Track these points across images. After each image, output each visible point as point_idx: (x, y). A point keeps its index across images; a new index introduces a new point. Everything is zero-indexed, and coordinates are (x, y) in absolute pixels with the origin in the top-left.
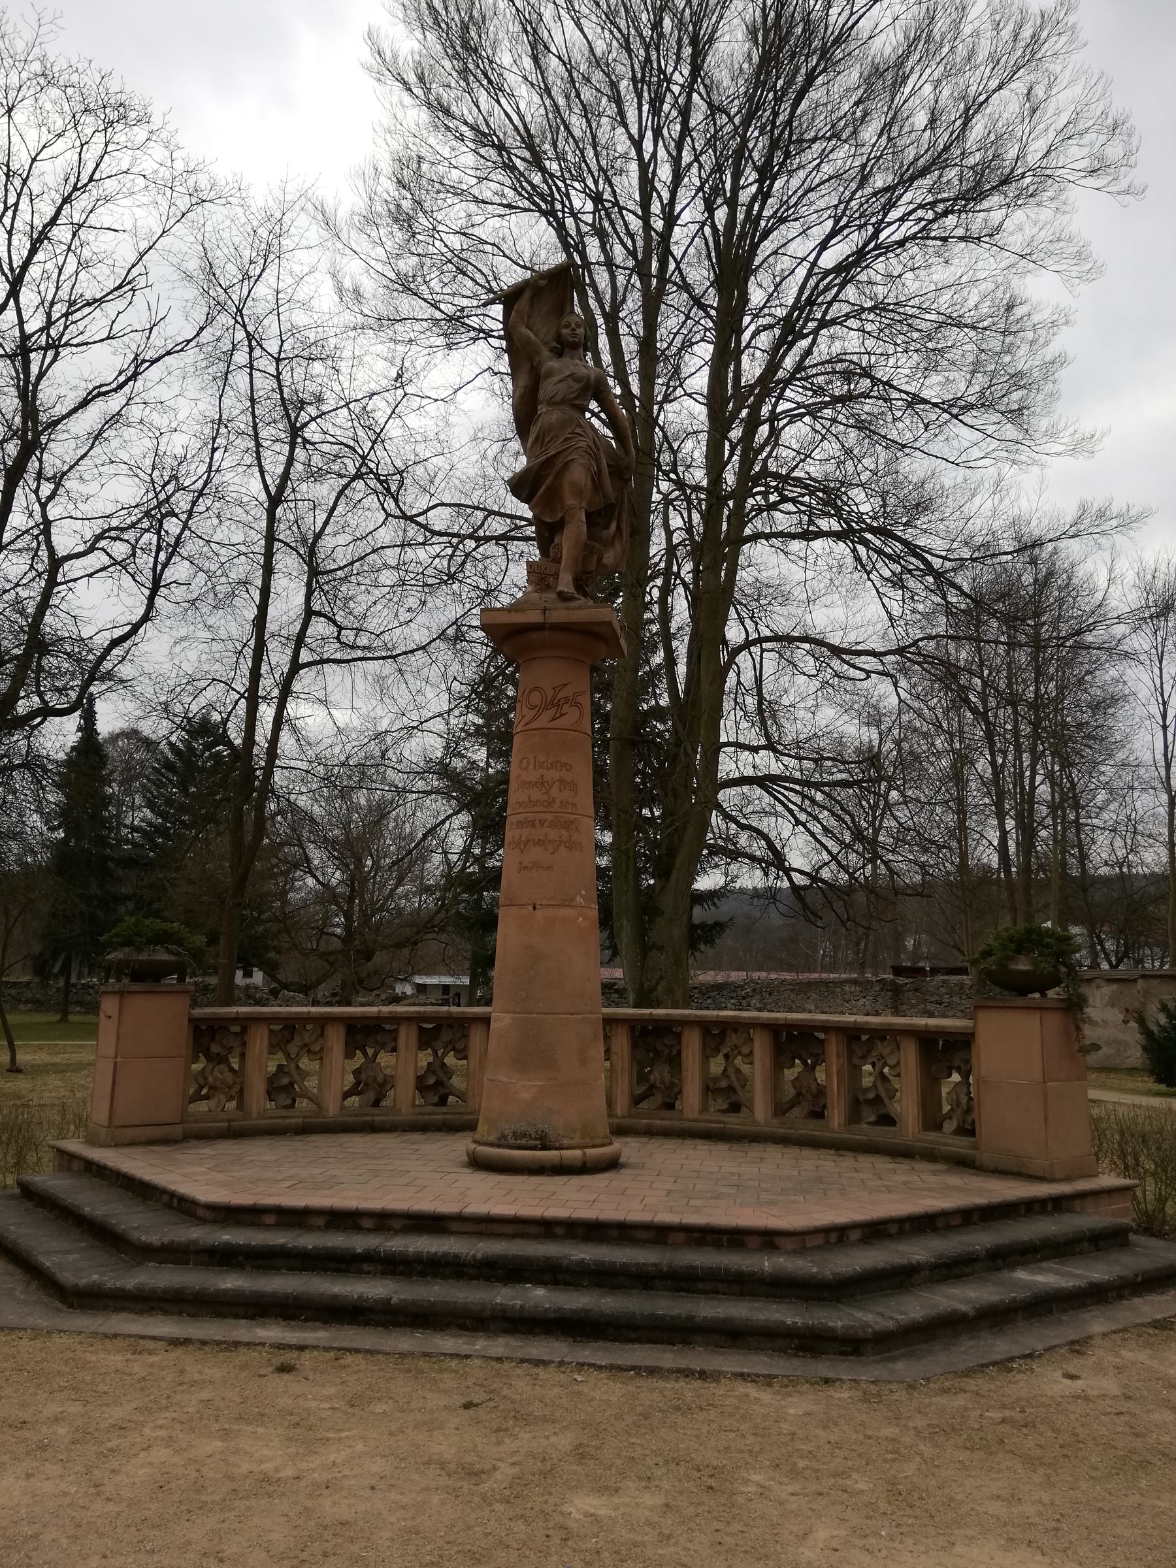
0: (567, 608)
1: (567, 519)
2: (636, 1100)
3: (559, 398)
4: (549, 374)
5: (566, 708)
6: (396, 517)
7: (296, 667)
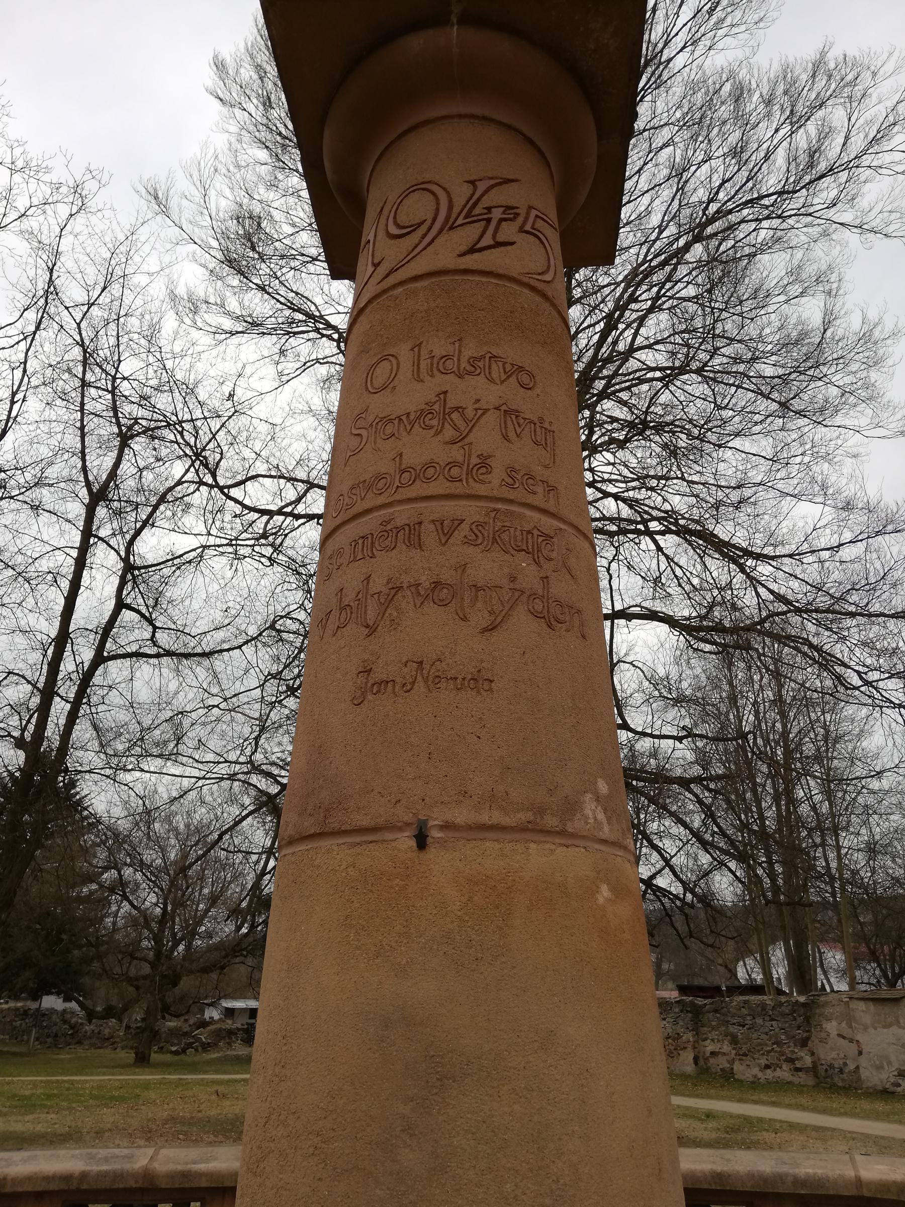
7: (99, 659)
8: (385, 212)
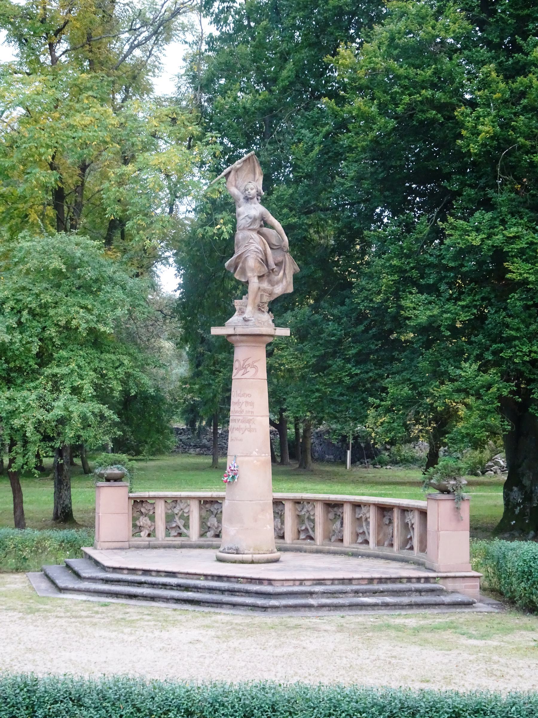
2: (202, 535)
5: (249, 369)
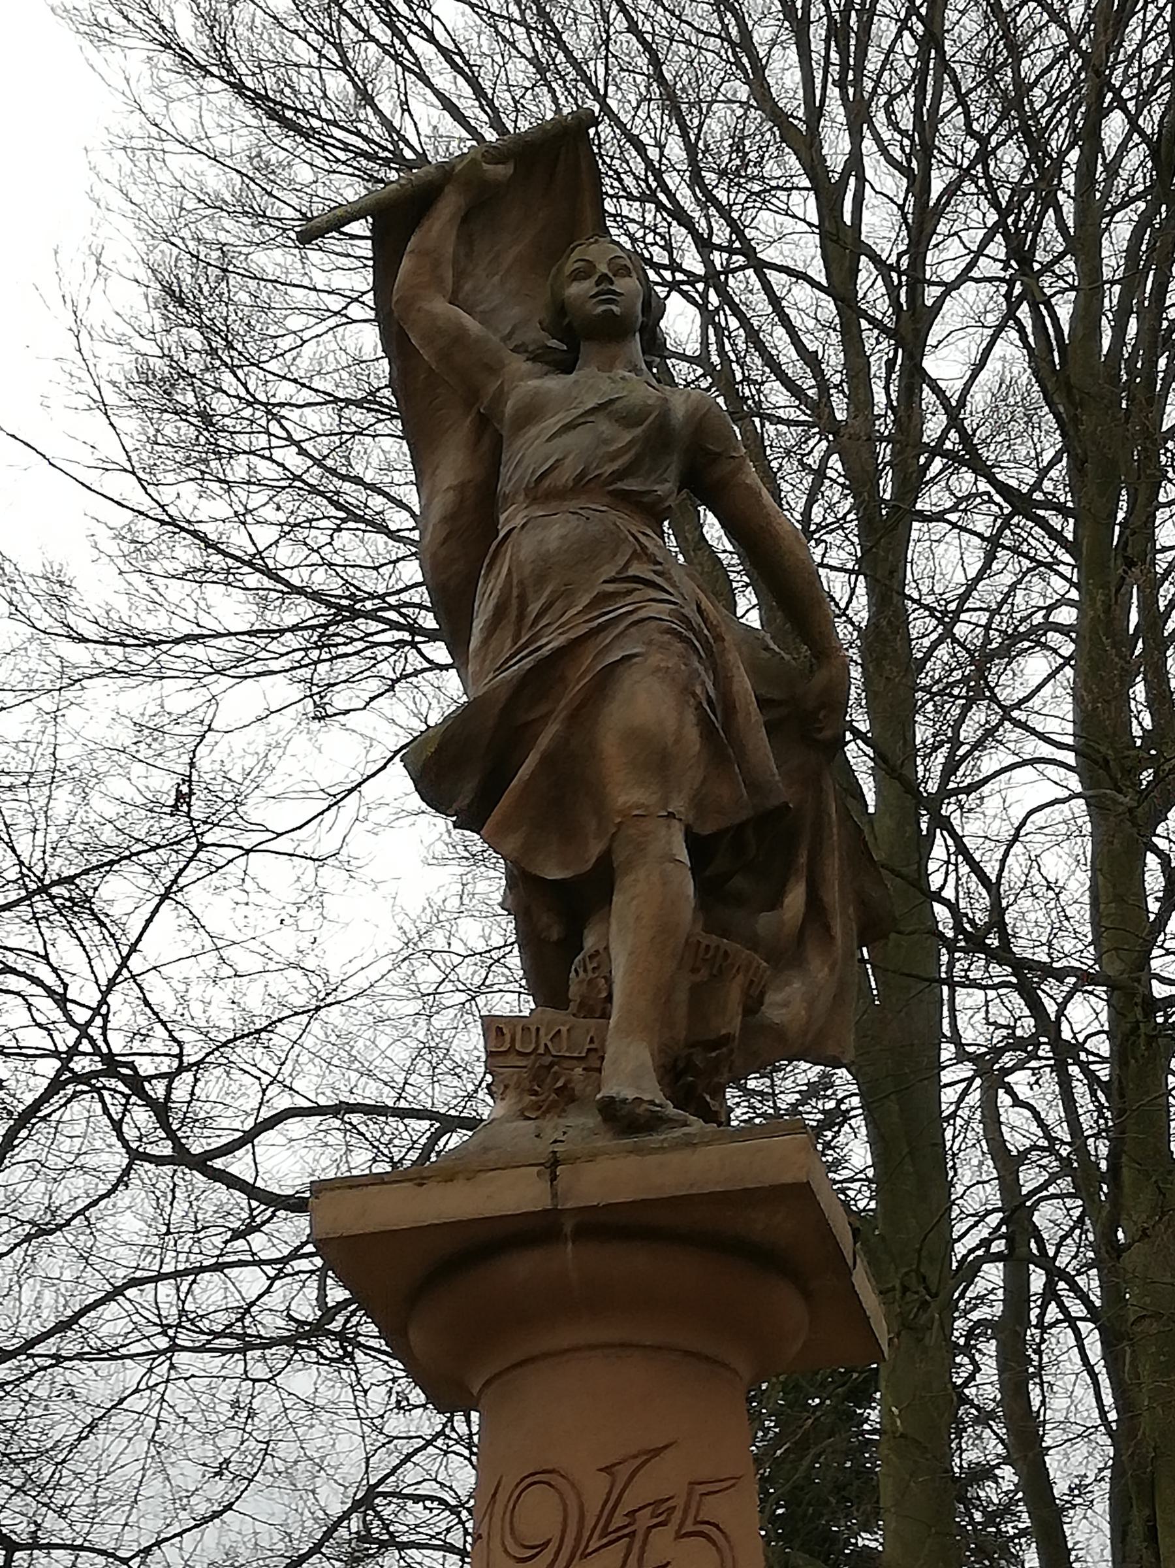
0: (637, 1151)
1: (619, 858)
3: (566, 475)
4: (530, 414)
6: (159, 1161)
8: (502, 1497)
